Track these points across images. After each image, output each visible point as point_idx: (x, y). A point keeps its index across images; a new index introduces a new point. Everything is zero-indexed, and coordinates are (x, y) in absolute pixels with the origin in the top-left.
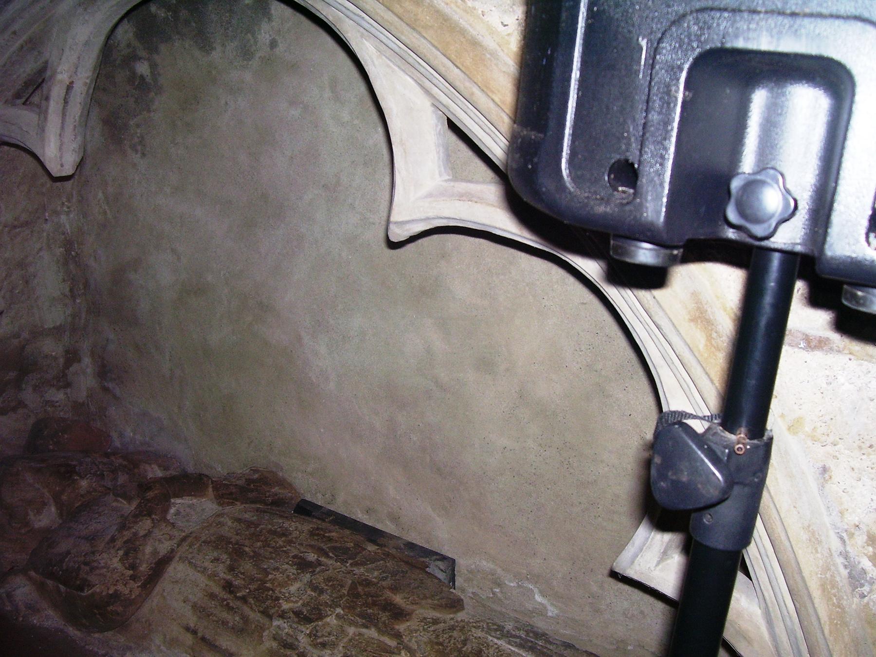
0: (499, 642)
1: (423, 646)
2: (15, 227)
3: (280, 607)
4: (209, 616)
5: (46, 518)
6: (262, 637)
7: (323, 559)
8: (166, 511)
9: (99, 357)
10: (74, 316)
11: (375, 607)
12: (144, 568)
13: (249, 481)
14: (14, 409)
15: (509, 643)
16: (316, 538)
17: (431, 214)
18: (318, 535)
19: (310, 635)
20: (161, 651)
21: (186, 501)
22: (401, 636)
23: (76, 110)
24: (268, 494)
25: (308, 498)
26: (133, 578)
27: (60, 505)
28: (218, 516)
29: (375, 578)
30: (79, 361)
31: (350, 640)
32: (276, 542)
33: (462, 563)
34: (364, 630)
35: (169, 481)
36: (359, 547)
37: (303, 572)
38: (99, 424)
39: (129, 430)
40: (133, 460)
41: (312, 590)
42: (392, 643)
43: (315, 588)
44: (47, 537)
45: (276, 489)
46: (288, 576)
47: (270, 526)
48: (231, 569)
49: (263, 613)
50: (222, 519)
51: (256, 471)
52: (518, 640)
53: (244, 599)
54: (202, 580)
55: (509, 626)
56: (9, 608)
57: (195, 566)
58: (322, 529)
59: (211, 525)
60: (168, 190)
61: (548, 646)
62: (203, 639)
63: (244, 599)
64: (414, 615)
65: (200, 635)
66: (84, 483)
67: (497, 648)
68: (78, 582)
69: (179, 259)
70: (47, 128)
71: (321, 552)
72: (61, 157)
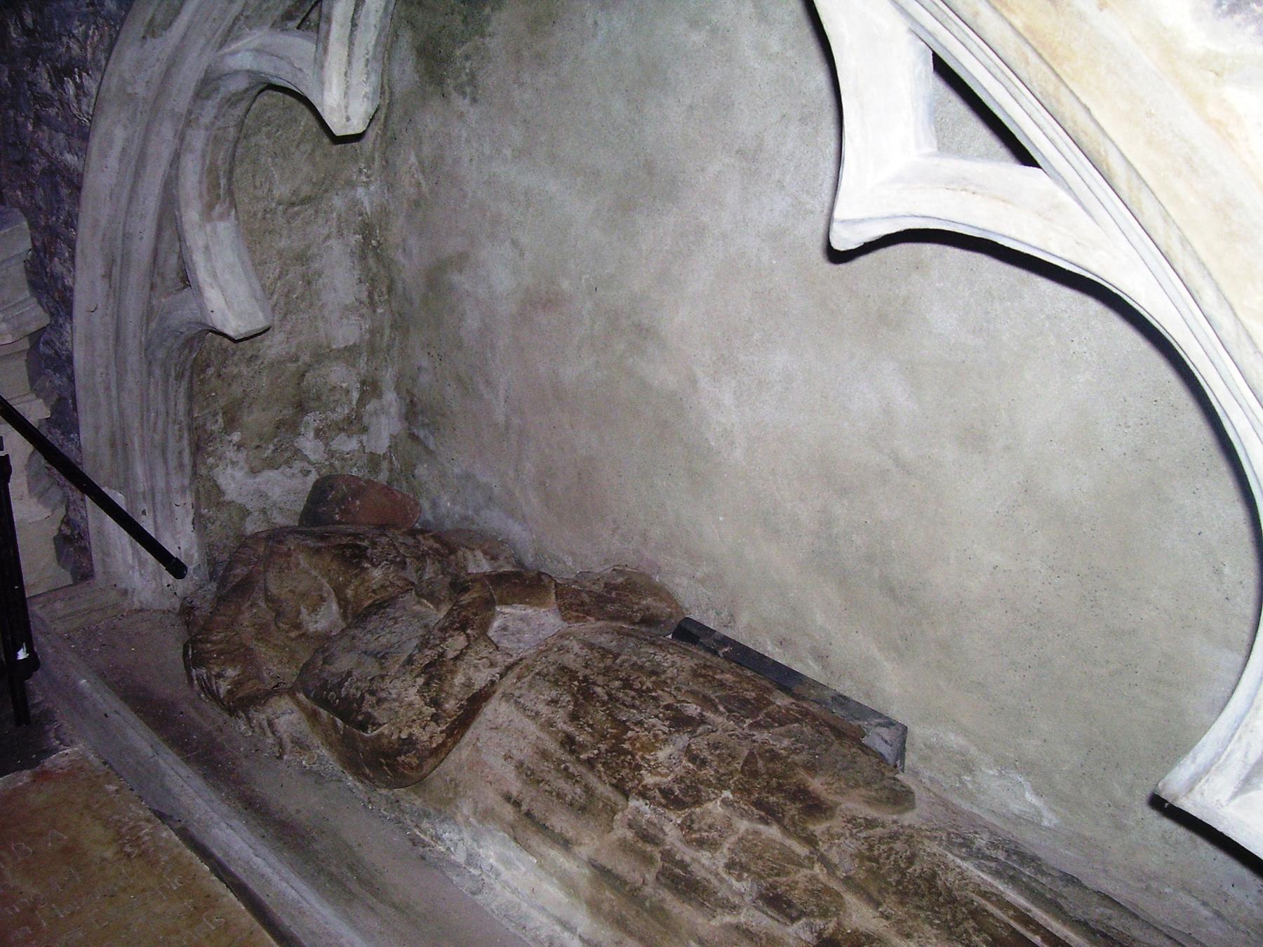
0: (964, 865)
2: (293, 204)
3: (640, 781)
4: (539, 782)
5: (325, 619)
6: (612, 820)
7: (709, 715)
8: (485, 626)
9: (408, 391)
10: (372, 332)
11: (782, 795)
12: (450, 705)
14: (288, 462)
15: (979, 867)
16: (701, 680)
17: (899, 210)
18: (704, 676)
19: (681, 827)
23: (368, 38)
24: (636, 607)
25: (696, 616)
26: (435, 718)
27: (343, 602)
28: (562, 637)
29: (784, 749)
30: (380, 396)
31: (741, 839)
33: (919, 733)
34: (761, 827)
35: (497, 579)
36: (761, 703)
39: (445, 498)
40: (447, 545)
41: (689, 761)
42: (802, 850)
43: (693, 758)
44: (323, 644)
45: (648, 601)
46: (656, 736)
47: (635, 658)
48: (574, 717)
50: (567, 642)
51: (621, 573)
52: (993, 864)
53: (590, 763)
54: (532, 728)
55: (981, 841)
58: (710, 667)
59: (551, 649)
60: (507, 152)
61: (1039, 877)
62: (528, 814)
63: (590, 763)
64: (838, 811)
65: (524, 808)
66: (377, 573)
67: (961, 873)
68: (360, 718)
69: (522, 255)
70: (326, 64)
71: (706, 702)
72: (346, 107)
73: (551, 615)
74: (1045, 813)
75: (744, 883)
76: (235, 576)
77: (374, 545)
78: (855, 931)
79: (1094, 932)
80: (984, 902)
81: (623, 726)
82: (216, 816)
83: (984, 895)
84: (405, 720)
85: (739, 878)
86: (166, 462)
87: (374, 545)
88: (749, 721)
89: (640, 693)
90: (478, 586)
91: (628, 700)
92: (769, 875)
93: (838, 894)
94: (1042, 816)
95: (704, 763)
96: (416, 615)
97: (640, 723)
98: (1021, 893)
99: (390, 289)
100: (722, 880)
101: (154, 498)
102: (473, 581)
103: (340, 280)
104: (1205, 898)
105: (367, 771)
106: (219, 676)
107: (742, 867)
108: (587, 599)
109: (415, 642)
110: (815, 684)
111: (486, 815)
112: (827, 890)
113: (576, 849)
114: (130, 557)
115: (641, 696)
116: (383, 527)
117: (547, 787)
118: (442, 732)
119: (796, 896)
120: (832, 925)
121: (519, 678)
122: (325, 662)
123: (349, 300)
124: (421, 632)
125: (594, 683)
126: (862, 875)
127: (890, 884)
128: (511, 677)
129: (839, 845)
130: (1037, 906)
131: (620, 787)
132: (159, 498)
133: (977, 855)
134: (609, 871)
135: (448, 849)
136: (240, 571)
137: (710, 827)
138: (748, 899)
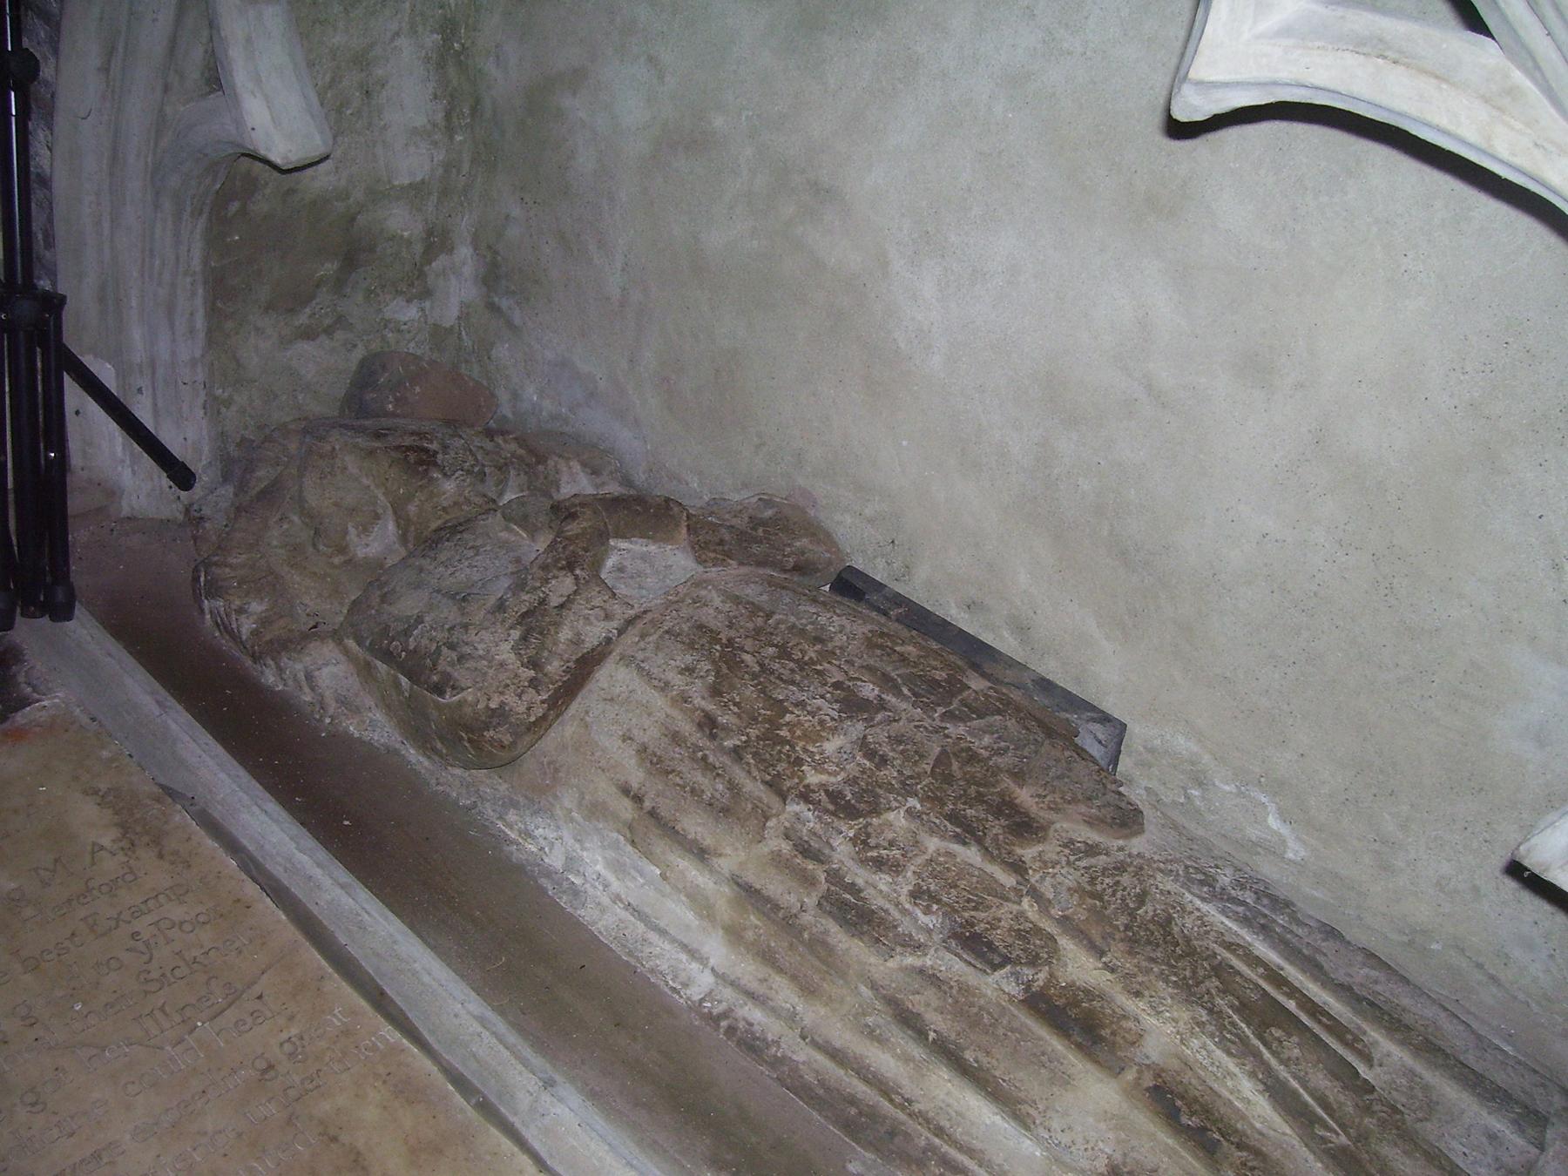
0: (1205, 907)
1: (1064, 895)
3: (801, 780)
4: (668, 773)
5: (378, 542)
7: (889, 697)
8: (597, 565)
10: (448, 166)
12: (554, 667)
13: (756, 522)
14: (329, 331)
15: (1223, 912)
16: (878, 652)
17: (1284, 75)
18: (881, 647)
19: (854, 840)
20: (572, 820)
21: (637, 546)
22: (1026, 870)
25: (859, 563)
26: (534, 683)
29: (985, 748)
30: (451, 251)
32: (803, 652)
33: (1138, 732)
34: (956, 848)
36: (954, 687)
37: (851, 717)
38: (476, 371)
40: (535, 451)
41: (865, 756)
42: (1008, 880)
43: (870, 754)
44: (377, 577)
45: (802, 543)
46: (822, 722)
47: (792, 619)
48: (715, 692)
49: (768, 784)
50: (703, 593)
51: (767, 503)
52: (1241, 909)
53: (737, 753)
54: (659, 702)
55: (1225, 879)
56: (308, 698)
57: (649, 676)
58: (888, 635)
61: (1294, 928)
62: (653, 813)
63: (737, 753)
64: (1051, 833)
66: (449, 486)
68: (435, 678)
69: (661, 78)
71: (886, 681)
73: (680, 555)
74: (1291, 843)
75: (934, 918)
76: (259, 479)
77: (445, 448)
78: (1071, 985)
79: (1359, 999)
80: (1227, 955)
81: (780, 707)
82: (246, 797)
83: (1229, 946)
84: (496, 684)
85: (927, 911)
86: (172, 326)
87: (445, 448)
88: (941, 710)
89: (802, 665)
90: (589, 512)
91: (786, 674)
92: (964, 909)
93: (1052, 938)
94: (1286, 847)
95: (883, 761)
96: (504, 545)
97: (801, 704)
98: (1274, 947)
99: (474, 110)
100: (904, 912)
101: (154, 373)
102: (582, 505)
103: (409, 97)
104: (1481, 960)
105: (439, 745)
106: (240, 611)
107: (930, 896)
108: (727, 537)
109: (505, 583)
110: (1011, 663)
111: (596, 810)
112: (1038, 931)
113: (715, 861)
114: (119, 449)
115: (802, 669)
116: (453, 424)
117: (677, 779)
118: (543, 702)
119: (997, 937)
120: (1042, 976)
121: (643, 636)
122: (384, 599)
123: (421, 121)
124: (511, 568)
125: (742, 649)
126: (1082, 915)
127: (1117, 928)
128: (631, 637)
129: (1054, 876)
130: (1291, 963)
131: (773, 785)
132: (160, 372)
133: (1219, 896)
134: (758, 892)
135: (542, 849)
136: (264, 475)
137: (892, 844)
138: (937, 938)
